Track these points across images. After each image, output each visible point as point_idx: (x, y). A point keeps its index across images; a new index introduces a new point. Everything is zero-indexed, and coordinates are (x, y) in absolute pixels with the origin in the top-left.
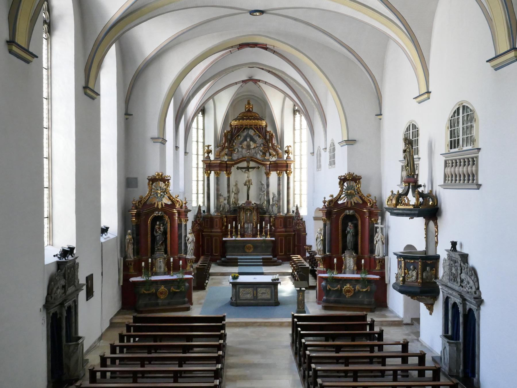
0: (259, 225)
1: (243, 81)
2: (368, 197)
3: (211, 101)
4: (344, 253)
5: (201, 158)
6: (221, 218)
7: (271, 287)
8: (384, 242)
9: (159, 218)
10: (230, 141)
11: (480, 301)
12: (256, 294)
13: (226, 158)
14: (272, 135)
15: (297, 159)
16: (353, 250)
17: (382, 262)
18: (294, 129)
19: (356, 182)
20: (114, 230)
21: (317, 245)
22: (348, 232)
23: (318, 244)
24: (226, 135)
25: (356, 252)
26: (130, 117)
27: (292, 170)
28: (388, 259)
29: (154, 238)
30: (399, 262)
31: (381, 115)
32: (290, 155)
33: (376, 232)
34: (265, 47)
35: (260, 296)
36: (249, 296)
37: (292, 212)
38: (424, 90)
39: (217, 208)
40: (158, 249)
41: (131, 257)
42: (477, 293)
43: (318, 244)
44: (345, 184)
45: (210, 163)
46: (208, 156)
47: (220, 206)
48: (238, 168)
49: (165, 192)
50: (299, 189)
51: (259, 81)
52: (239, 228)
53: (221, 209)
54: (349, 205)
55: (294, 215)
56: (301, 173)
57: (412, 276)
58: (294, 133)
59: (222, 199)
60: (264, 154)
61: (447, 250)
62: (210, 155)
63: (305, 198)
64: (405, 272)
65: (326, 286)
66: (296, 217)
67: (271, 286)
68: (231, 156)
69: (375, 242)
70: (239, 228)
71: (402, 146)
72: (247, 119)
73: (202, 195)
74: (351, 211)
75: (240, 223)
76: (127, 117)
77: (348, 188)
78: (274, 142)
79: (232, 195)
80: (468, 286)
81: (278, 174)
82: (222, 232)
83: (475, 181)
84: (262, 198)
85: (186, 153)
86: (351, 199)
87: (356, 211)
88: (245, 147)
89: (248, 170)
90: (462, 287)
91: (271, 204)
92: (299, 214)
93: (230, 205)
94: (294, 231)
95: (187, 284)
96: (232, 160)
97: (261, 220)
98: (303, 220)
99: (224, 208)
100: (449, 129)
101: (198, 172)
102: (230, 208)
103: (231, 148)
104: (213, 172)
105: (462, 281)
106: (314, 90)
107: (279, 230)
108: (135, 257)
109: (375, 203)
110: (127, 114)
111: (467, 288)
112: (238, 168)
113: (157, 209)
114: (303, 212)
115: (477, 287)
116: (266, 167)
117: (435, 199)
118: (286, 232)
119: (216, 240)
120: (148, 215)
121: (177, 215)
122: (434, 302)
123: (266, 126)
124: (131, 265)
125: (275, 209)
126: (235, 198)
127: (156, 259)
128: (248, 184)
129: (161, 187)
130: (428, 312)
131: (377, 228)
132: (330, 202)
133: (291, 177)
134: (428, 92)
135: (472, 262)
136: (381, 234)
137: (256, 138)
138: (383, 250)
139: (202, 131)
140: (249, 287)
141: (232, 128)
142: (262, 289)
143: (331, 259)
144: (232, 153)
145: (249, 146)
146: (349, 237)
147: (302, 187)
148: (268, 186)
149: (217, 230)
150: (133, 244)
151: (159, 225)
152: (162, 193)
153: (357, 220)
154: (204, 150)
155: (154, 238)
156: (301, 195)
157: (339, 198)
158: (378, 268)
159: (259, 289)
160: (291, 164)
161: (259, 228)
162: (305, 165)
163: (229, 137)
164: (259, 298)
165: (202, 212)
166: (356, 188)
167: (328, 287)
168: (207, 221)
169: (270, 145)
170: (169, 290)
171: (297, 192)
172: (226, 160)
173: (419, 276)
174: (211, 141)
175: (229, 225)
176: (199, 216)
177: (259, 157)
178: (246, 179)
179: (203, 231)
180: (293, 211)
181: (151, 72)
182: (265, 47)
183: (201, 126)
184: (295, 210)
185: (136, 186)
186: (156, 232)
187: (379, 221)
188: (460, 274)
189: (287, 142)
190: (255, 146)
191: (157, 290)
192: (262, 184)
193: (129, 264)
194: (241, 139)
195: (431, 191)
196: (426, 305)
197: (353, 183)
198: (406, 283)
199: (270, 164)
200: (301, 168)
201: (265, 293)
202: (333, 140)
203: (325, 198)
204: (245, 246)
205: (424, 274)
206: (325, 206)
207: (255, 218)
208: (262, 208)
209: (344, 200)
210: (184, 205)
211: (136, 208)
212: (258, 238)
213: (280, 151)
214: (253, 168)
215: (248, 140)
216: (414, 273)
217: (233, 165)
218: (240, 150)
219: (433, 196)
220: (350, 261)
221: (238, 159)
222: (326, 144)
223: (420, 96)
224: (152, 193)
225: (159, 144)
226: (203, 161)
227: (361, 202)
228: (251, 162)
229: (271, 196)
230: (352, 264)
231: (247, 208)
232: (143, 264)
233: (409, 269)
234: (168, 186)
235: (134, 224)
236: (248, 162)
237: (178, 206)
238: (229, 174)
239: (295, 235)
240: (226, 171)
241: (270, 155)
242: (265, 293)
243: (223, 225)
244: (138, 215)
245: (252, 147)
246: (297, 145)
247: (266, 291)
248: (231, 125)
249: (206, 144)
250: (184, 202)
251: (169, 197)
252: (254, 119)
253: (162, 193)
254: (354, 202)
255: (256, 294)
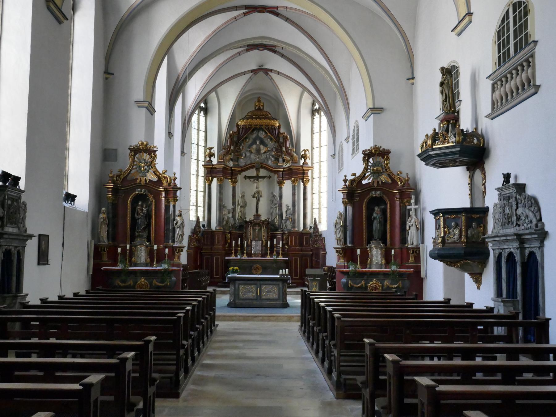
0: (269, 242)
1: (252, 71)
2: (398, 175)
3: (213, 94)
4: (370, 243)
5: (201, 163)
6: (224, 233)
7: (279, 284)
8: (419, 226)
9: (142, 198)
10: (237, 144)
11: (543, 235)
12: (260, 293)
13: (231, 164)
14: (286, 137)
15: (316, 166)
16: (380, 240)
17: (416, 252)
18: (313, 133)
19: (383, 158)
20: (83, 200)
21: (336, 232)
22: (375, 218)
23: (338, 232)
24: (231, 137)
25: (384, 241)
26: (111, 77)
27: (310, 178)
28: (423, 247)
29: (134, 221)
30: (437, 221)
31: (413, 78)
32: (307, 161)
33: (409, 216)
34: (273, 11)
35: (265, 296)
36: (251, 295)
37: (309, 228)
38: (464, 12)
39: (220, 221)
40: (139, 235)
41: (105, 241)
42: (539, 225)
43: (338, 232)
44: (371, 160)
45: (212, 168)
46: (210, 159)
47: (223, 219)
48: (245, 177)
49: (150, 165)
50: (318, 202)
51: (271, 70)
52: (245, 246)
53: (225, 223)
54: (376, 184)
55: (312, 231)
56: (320, 183)
57: (454, 235)
58: (313, 136)
59: (225, 212)
60: (277, 160)
61: (498, 189)
62: (212, 158)
63: (324, 213)
64: (444, 231)
65: (347, 283)
66: (314, 233)
67: (278, 283)
68: (237, 161)
69: (408, 228)
70: (245, 246)
71: (439, 77)
72: (256, 119)
73: (202, 209)
74: (378, 192)
75: (247, 240)
76: (108, 76)
77: (374, 165)
78: (288, 146)
79: (238, 209)
80: (527, 221)
81: (293, 182)
82: (224, 250)
83: (531, 84)
84: (274, 212)
85: (183, 153)
86: (378, 177)
87: (384, 192)
88: (253, 151)
89: (258, 180)
90: (519, 225)
91: (284, 218)
92: (318, 229)
93: (235, 220)
94: (311, 250)
95: (174, 278)
96: (238, 166)
97: (272, 237)
98: (323, 236)
99: (227, 223)
100: (497, 43)
101: (197, 169)
102: (235, 223)
103: (237, 152)
104: (215, 180)
105: (518, 219)
106: (334, 68)
107: (293, 248)
108: (110, 243)
109: (408, 180)
110: (106, 72)
111: (525, 225)
112: (245, 177)
113: (140, 186)
114: (323, 227)
115: (538, 218)
116: (278, 175)
117: (481, 137)
118: (302, 251)
119: (217, 259)
120: (127, 193)
121: (163, 195)
122: (483, 271)
123: (279, 127)
124: (104, 251)
125: (289, 224)
126: (241, 212)
127: (136, 246)
128: (257, 196)
129: (145, 160)
130: (475, 285)
131: (410, 210)
132: (352, 181)
133: (309, 186)
134: (470, 14)
135: (530, 191)
136: (415, 217)
137: (268, 141)
138: (417, 236)
139: (204, 133)
140: (251, 284)
141: (239, 129)
142: (267, 286)
143: (353, 250)
144: (238, 158)
145: (258, 151)
146: (376, 225)
147: (322, 199)
148: (281, 197)
149: (219, 247)
150: (108, 225)
151: (142, 206)
152: (146, 167)
153: (385, 204)
154: (205, 151)
155: (134, 221)
156: (320, 209)
157: (363, 176)
158: (411, 260)
159: (263, 287)
160: (308, 170)
161: (269, 246)
162: (324, 173)
163: (235, 139)
164: (264, 297)
165: (201, 226)
166: (384, 165)
167: (350, 283)
168: (207, 237)
169: (284, 149)
170: (151, 284)
171: (316, 206)
172: (231, 165)
173: (463, 234)
174: (214, 143)
175: (234, 242)
176: (198, 230)
177: (270, 163)
178: (255, 190)
179: (201, 249)
180: (311, 227)
181: (138, 25)
182: (273, 11)
183: (202, 127)
184: (313, 225)
185: (116, 160)
186: (138, 214)
187: (413, 201)
188: (516, 210)
189: (304, 145)
190: (266, 151)
191: (135, 283)
192: (274, 196)
193: (101, 250)
194: (250, 142)
195: (476, 129)
196: (472, 275)
197: (380, 159)
198: (446, 245)
199: (283, 171)
200: (320, 177)
201: (271, 292)
202: (357, 121)
203: (346, 176)
204: (251, 267)
205: (469, 232)
206: (345, 185)
207: (264, 234)
208: (274, 225)
209: (369, 179)
210: (173, 182)
211: (113, 182)
212: (269, 257)
213: (295, 155)
214: (263, 177)
215: (258, 142)
216: (457, 231)
217: (240, 172)
218: (248, 154)
219: (479, 135)
220: (376, 255)
221: (246, 165)
222: (348, 133)
223: (460, 22)
224: (134, 167)
225: (145, 109)
226: (203, 165)
227: (390, 181)
228: (261, 170)
229: (284, 209)
230: (379, 257)
231: (256, 223)
232: (119, 250)
233: (449, 228)
234: (154, 158)
235: (110, 201)
236: (258, 170)
237: (164, 182)
238: (234, 182)
239: (312, 254)
240: (231, 179)
241: (284, 161)
242: (271, 292)
243: (226, 242)
244: (115, 191)
245: (262, 151)
246: (316, 151)
247: (272, 288)
248: (238, 126)
249: (208, 146)
250: (173, 178)
251: (154, 172)
252: (265, 118)
253: (146, 167)
254: (382, 182)
255: (260, 293)
